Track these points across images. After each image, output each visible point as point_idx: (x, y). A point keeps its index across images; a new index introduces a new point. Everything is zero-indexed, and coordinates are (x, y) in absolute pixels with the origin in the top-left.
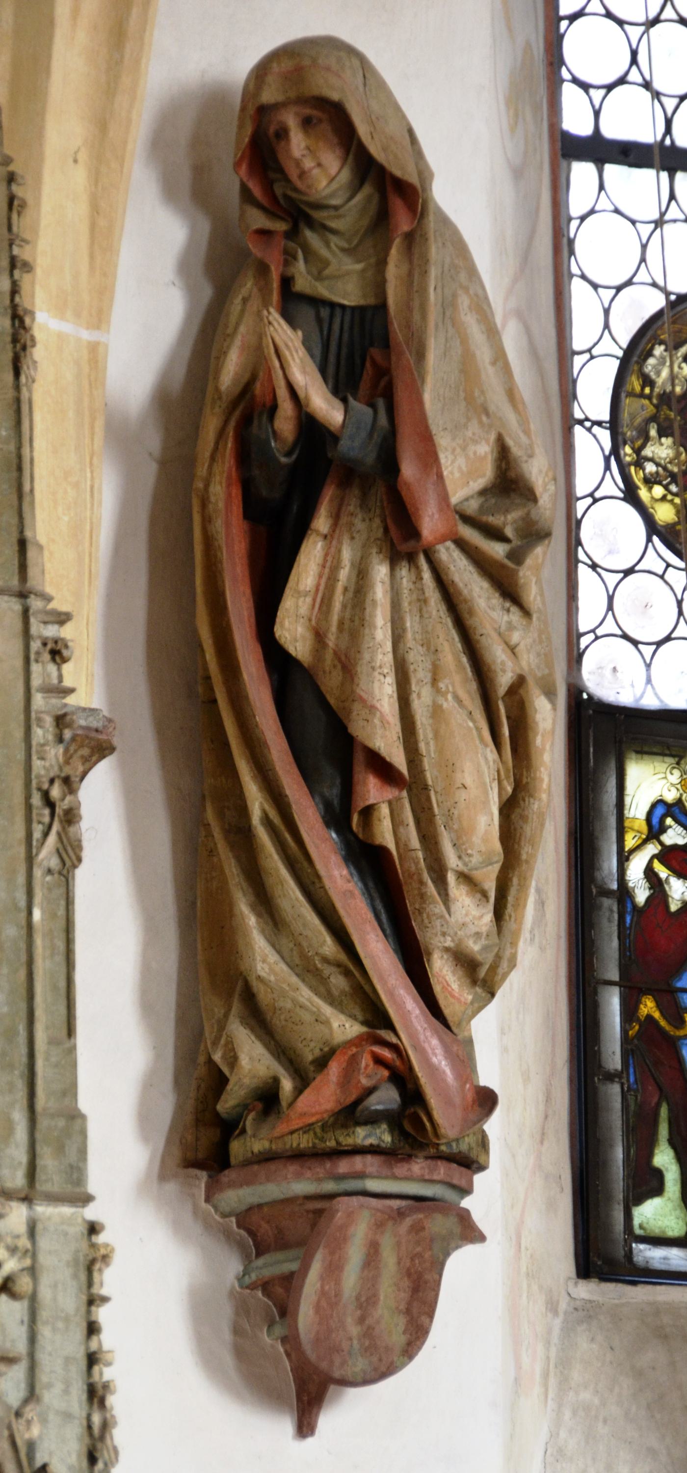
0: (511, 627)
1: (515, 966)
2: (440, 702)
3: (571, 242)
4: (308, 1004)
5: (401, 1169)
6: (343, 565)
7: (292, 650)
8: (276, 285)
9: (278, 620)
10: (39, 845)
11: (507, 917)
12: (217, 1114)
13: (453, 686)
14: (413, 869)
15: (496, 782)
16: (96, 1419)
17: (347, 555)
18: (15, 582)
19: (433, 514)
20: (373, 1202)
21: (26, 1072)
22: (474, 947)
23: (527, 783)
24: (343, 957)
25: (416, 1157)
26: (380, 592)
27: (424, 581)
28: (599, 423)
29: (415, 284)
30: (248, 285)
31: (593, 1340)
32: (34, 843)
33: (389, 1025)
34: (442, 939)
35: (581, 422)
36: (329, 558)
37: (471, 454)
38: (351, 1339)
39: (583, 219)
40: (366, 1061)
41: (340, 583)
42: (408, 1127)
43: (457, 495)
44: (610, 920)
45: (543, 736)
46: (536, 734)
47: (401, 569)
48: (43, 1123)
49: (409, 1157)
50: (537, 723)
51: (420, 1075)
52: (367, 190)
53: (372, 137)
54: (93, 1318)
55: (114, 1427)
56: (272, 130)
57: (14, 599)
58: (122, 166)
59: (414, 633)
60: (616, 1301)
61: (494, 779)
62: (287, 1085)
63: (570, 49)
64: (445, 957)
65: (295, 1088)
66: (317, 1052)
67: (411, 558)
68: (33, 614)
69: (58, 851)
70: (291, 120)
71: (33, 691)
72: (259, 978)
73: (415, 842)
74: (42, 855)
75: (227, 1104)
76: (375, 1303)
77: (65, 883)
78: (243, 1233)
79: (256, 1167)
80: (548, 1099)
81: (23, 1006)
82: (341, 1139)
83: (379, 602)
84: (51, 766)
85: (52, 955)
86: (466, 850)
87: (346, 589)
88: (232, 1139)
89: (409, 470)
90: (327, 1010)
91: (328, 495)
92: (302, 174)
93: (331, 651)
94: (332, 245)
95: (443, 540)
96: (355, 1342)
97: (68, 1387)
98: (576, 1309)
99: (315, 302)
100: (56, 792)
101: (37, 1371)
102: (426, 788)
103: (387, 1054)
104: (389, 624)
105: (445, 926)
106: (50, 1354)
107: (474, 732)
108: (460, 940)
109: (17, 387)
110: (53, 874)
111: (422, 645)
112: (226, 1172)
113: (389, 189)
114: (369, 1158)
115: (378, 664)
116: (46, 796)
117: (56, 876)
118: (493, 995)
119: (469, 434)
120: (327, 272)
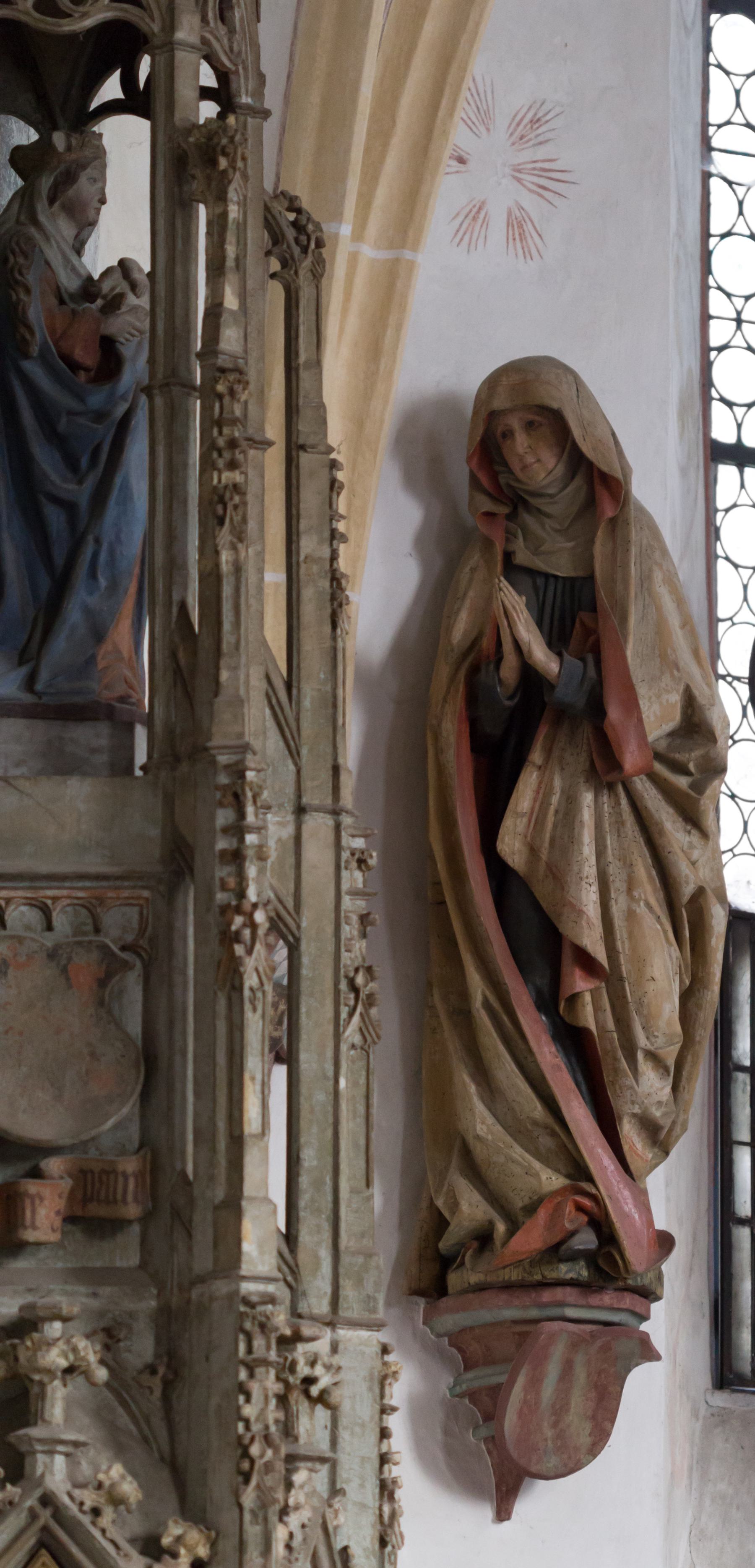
0: (691, 846)
1: (686, 1130)
2: (634, 908)
3: (717, 530)
4: (520, 1159)
5: (594, 1300)
6: (554, 792)
7: (510, 862)
8: (499, 558)
9: (500, 836)
10: (346, 1023)
11: (682, 1089)
12: (437, 1250)
13: (645, 895)
14: (609, 1048)
15: (678, 975)
16: (386, 1509)
17: (557, 783)
18: (329, 801)
19: (634, 751)
20: (571, 1326)
21: (332, 1216)
22: (657, 1113)
23: (703, 977)
24: (550, 1121)
25: (607, 1289)
26: (587, 815)
27: (622, 806)
28: (738, 679)
29: (618, 559)
30: (475, 558)
31: (727, 1440)
32: (342, 1022)
33: (590, 1179)
34: (631, 1107)
35: (723, 677)
36: (543, 786)
37: (664, 702)
38: (546, 1440)
39: (727, 511)
40: (569, 1208)
41: (552, 806)
42: (601, 1263)
43: (652, 735)
44: (744, 1091)
45: (717, 938)
46: (711, 938)
47: (603, 796)
48: (345, 1260)
49: (601, 1289)
50: (712, 927)
51: (615, 1220)
52: (578, 481)
53: (584, 440)
54: (384, 1425)
55: (401, 1516)
56: (500, 430)
57: (328, 816)
58: (375, 457)
59: (612, 850)
60: (745, 1409)
61: (676, 973)
62: (501, 1228)
63: (718, 374)
64: (633, 1121)
65: (508, 1230)
66: (527, 1201)
67: (611, 787)
68: (344, 829)
69: (361, 1029)
70: (515, 423)
71: (343, 894)
72: (478, 1137)
73: (611, 1025)
74: (347, 1033)
75: (444, 1245)
76: (568, 1410)
77: (366, 1057)
78: (454, 1351)
79: (471, 1296)
80: (695, 1239)
81: (329, 1160)
82: (546, 1273)
83: (586, 823)
84: (356, 957)
85: (354, 1118)
86: (653, 1032)
87: (557, 812)
88: (450, 1271)
89: (614, 713)
90: (537, 1165)
91: (543, 732)
92: (525, 468)
93: (544, 864)
94: (547, 527)
95: (638, 774)
96: (550, 1442)
97: (364, 1482)
98: (713, 1415)
99: (532, 573)
100: (360, 980)
101: (338, 1468)
102: (621, 979)
103: (587, 1202)
104: (594, 842)
105: (634, 1096)
106: (349, 1454)
107: (662, 933)
108: (646, 1108)
109: (334, 638)
110: (356, 1049)
111: (619, 860)
112: (444, 1299)
113: (597, 481)
114: (568, 1290)
115: (585, 875)
116: (352, 983)
117: (359, 1050)
118: (667, 1153)
119: (663, 685)
120: (543, 548)
